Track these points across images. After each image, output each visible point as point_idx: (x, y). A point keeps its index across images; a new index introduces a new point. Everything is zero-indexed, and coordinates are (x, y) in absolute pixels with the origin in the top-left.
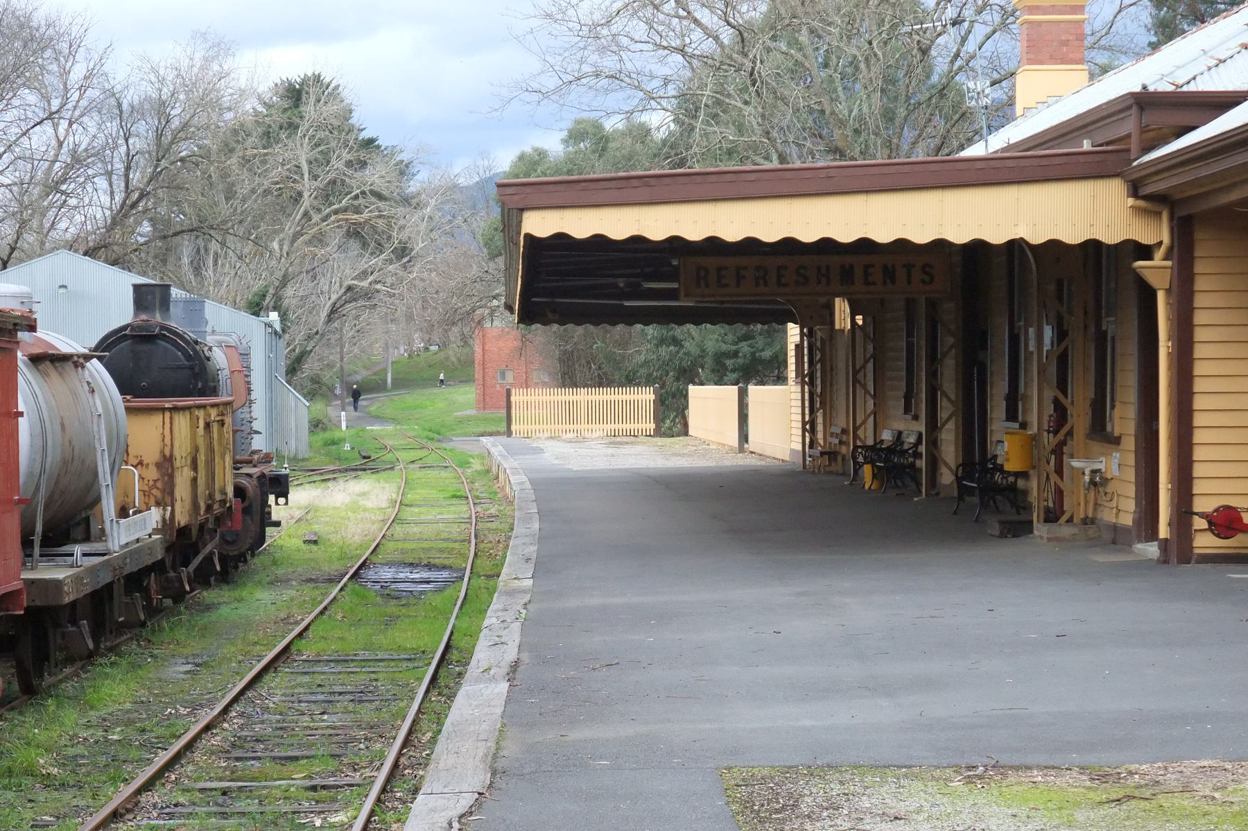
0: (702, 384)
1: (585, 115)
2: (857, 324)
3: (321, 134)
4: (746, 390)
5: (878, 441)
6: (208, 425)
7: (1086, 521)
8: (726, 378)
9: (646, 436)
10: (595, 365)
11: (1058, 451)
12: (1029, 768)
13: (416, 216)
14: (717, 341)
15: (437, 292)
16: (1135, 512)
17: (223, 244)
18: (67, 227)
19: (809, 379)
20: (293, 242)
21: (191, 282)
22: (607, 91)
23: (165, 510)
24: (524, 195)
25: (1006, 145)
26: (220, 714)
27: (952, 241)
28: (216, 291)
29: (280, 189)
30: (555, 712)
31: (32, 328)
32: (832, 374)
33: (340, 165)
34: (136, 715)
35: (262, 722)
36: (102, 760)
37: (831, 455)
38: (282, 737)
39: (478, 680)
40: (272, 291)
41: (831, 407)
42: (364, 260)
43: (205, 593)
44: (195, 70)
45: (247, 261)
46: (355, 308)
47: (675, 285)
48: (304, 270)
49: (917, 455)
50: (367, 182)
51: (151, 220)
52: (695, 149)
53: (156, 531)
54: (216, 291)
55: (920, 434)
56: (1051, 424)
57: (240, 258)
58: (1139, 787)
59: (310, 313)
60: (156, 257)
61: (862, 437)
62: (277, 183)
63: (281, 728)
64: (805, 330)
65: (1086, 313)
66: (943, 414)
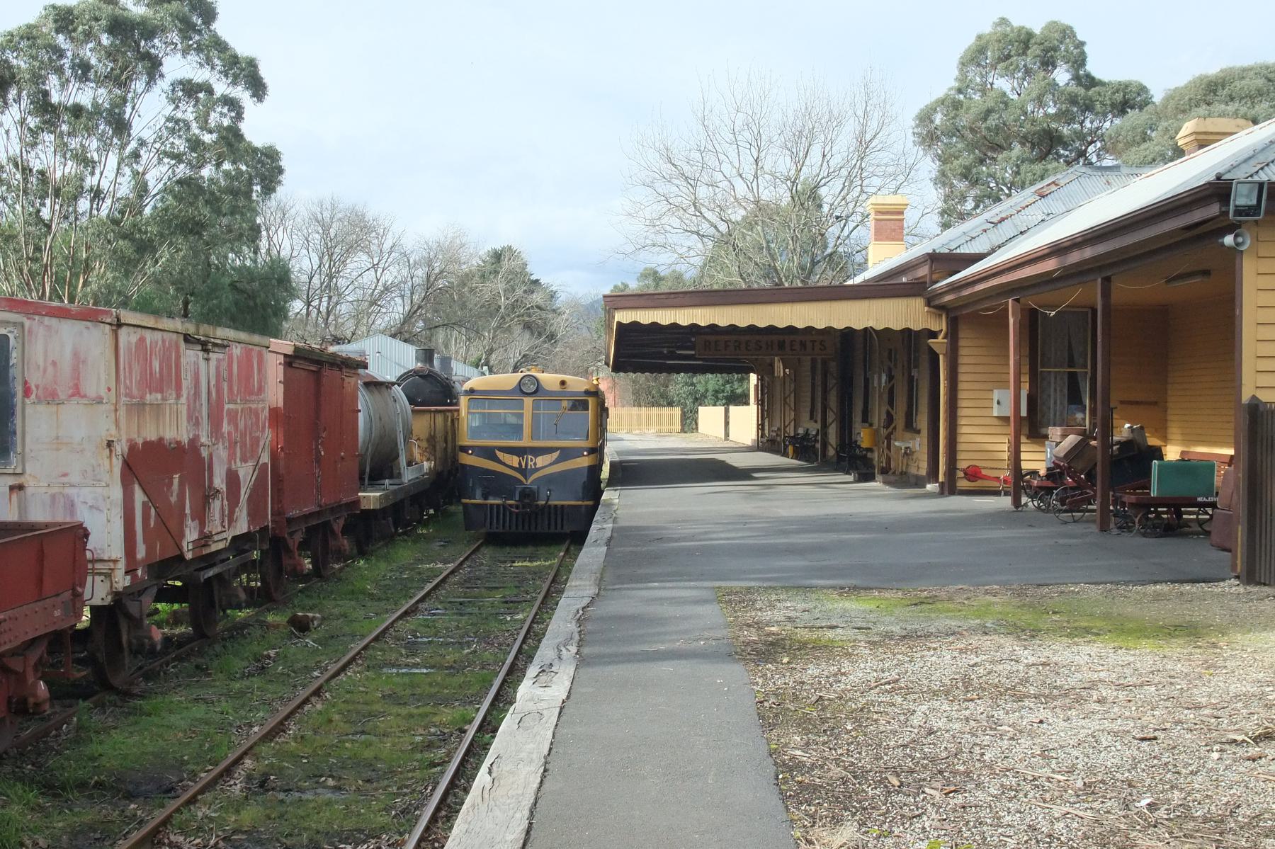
1: (648, 266)
11: (888, 438)
12: (872, 589)
18: (381, 323)
22: (658, 254)
31: (366, 367)
33: (521, 292)
36: (399, 587)
44: (448, 243)
47: (693, 353)
49: (816, 441)
53: (427, 474)
55: (818, 430)
58: (926, 598)
60: (426, 338)
66: (829, 420)
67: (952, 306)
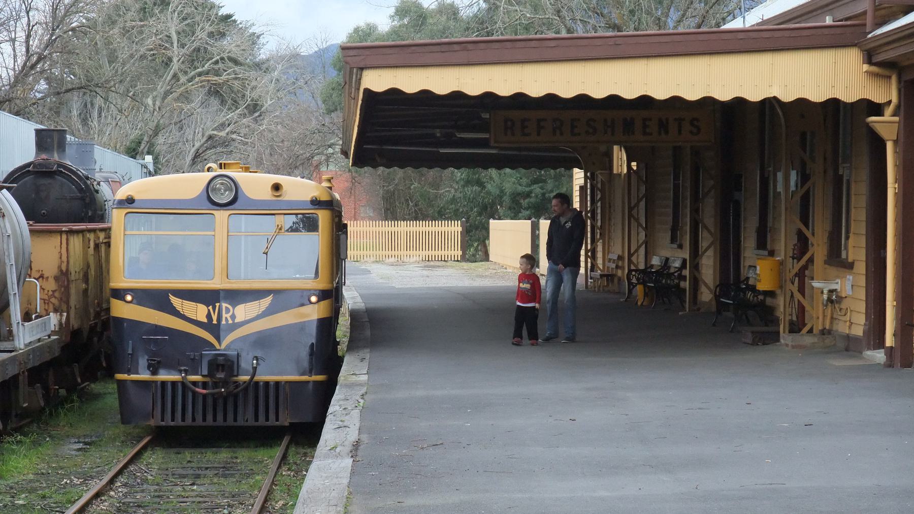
0: (500, 219)
2: (633, 169)
3: (188, 10)
4: (538, 223)
5: (648, 266)
6: (97, 246)
7: (824, 332)
8: (520, 214)
9: (454, 261)
10: (412, 202)
11: (801, 275)
13: (266, 78)
14: (514, 183)
15: (283, 141)
16: (865, 324)
17: (106, 99)
19: (591, 214)
20: (164, 98)
21: (79, 131)
23: (61, 315)
24: (363, 57)
25: (761, 20)
26: (107, 484)
27: (718, 98)
28: (100, 138)
29: (154, 55)
30: (392, 482)
32: (610, 212)
33: (204, 35)
34: (37, 484)
35: (143, 491)
37: (609, 277)
38: (159, 503)
39: (326, 457)
40: (146, 139)
41: (609, 238)
42: (223, 114)
43: (93, 386)
45: (126, 114)
46: (215, 154)
47: (486, 136)
48: (173, 122)
50: (226, 50)
51: (47, 79)
52: (499, 24)
53: (54, 333)
54: (100, 138)
55: (684, 261)
56: (795, 252)
57: (120, 111)
59: (178, 157)
61: (635, 262)
62: (152, 50)
63: (158, 497)
64: (588, 174)
65: (825, 159)
67: (907, 63)
